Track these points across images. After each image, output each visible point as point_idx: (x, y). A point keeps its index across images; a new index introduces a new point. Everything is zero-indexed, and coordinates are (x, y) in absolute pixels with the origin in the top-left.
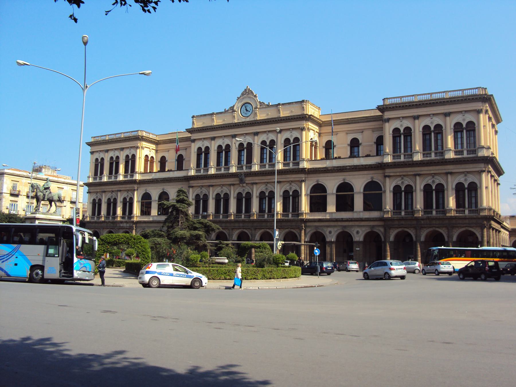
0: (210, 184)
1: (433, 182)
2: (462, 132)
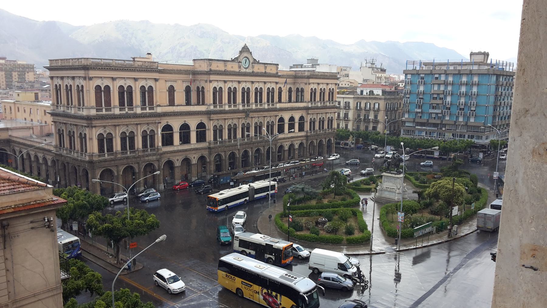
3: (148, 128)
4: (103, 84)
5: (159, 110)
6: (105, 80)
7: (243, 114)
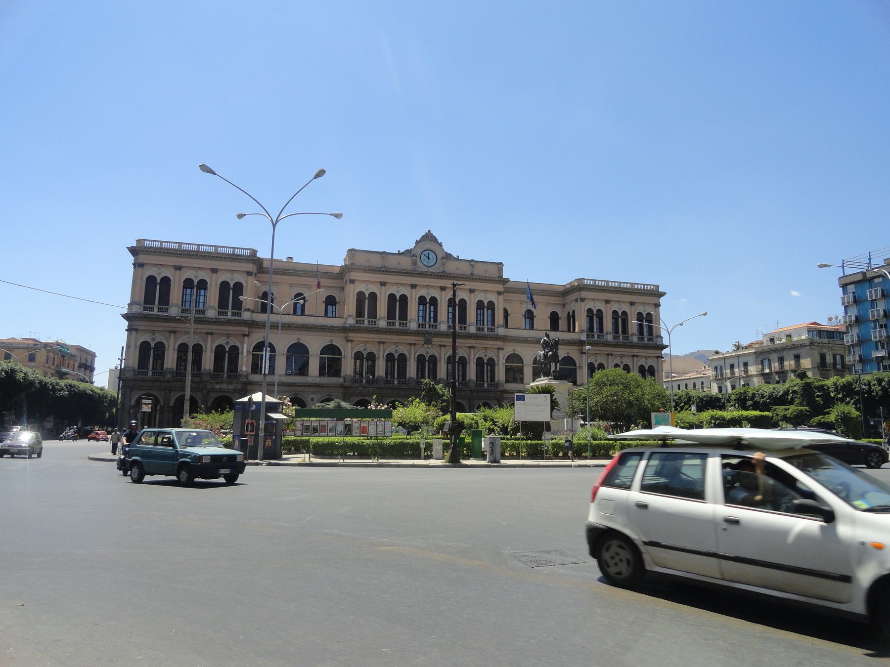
1: (227, 343)
2: (192, 288)
3: (227, 343)
4: (159, 274)
5: (246, 316)
6: (236, 275)
7: (422, 338)
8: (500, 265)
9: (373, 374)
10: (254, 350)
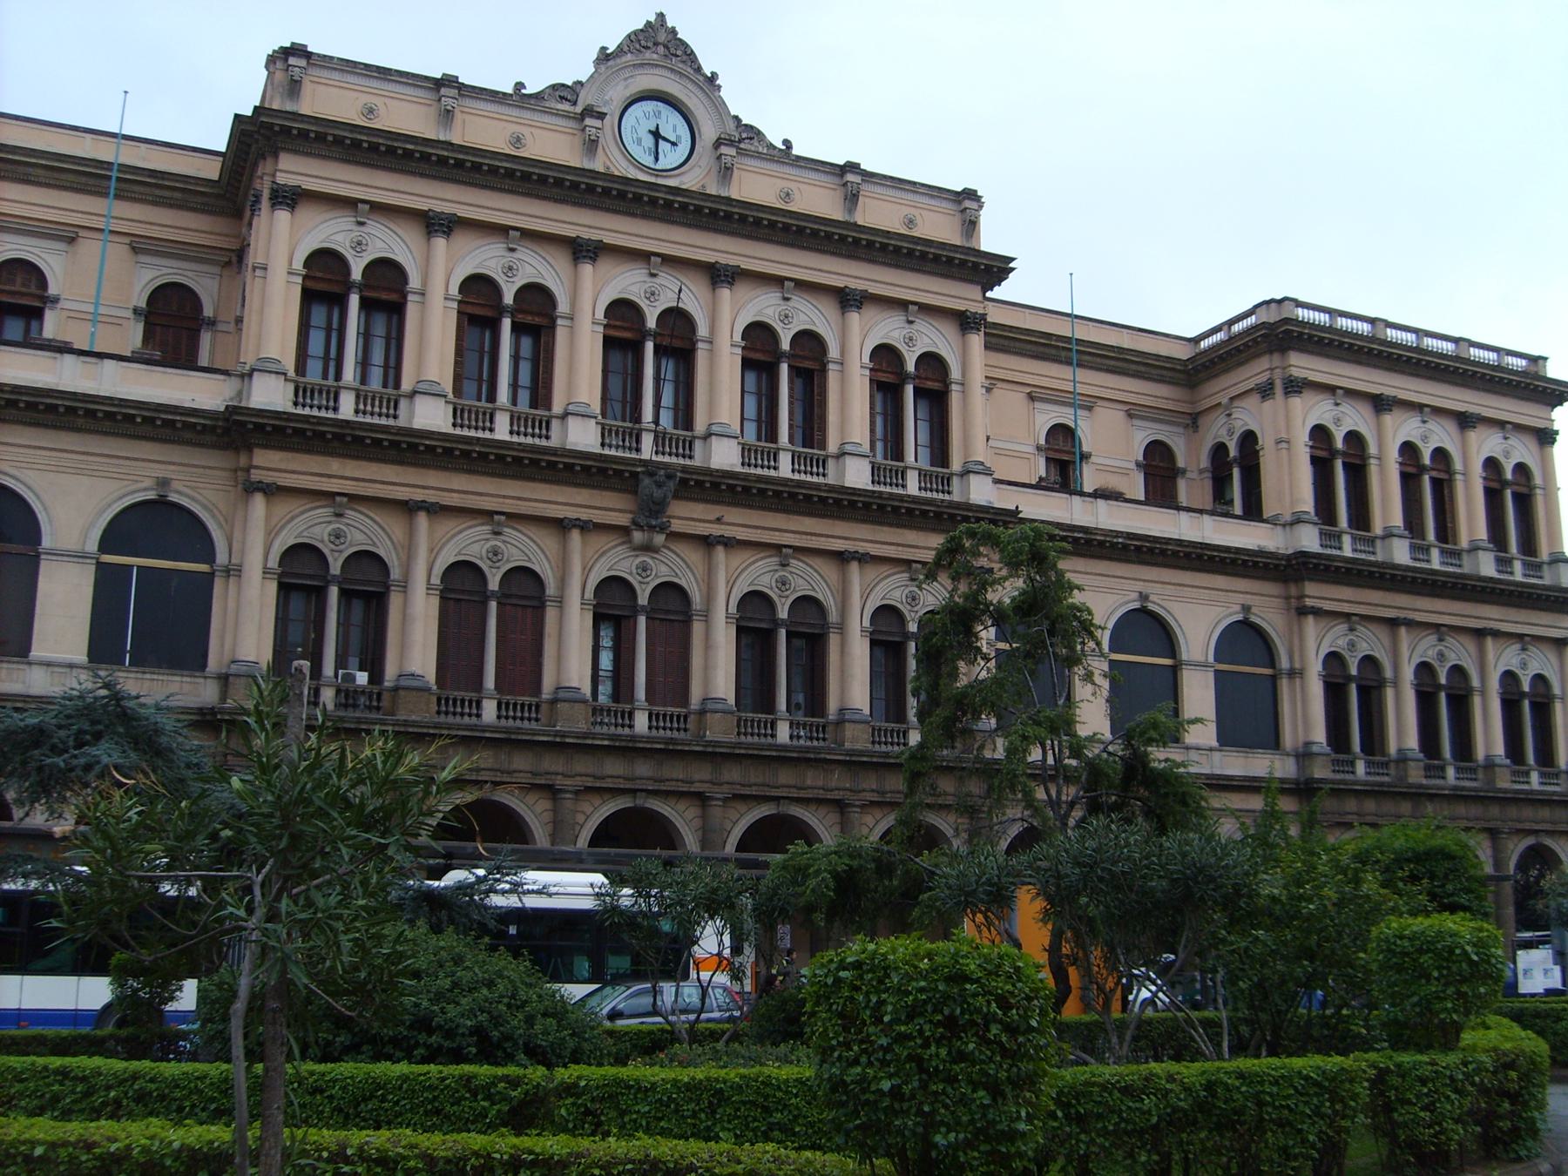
0: (418, 495)
8: (966, 202)
9: (374, 662)
10: (106, 544)
